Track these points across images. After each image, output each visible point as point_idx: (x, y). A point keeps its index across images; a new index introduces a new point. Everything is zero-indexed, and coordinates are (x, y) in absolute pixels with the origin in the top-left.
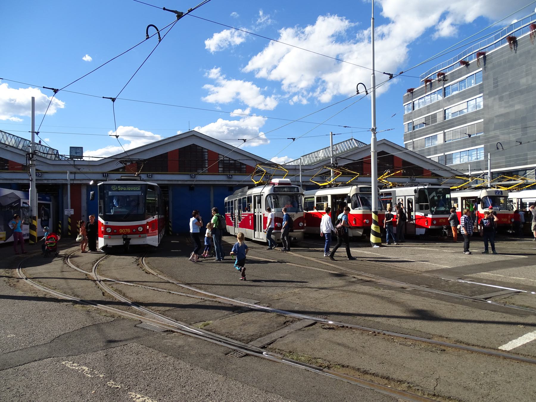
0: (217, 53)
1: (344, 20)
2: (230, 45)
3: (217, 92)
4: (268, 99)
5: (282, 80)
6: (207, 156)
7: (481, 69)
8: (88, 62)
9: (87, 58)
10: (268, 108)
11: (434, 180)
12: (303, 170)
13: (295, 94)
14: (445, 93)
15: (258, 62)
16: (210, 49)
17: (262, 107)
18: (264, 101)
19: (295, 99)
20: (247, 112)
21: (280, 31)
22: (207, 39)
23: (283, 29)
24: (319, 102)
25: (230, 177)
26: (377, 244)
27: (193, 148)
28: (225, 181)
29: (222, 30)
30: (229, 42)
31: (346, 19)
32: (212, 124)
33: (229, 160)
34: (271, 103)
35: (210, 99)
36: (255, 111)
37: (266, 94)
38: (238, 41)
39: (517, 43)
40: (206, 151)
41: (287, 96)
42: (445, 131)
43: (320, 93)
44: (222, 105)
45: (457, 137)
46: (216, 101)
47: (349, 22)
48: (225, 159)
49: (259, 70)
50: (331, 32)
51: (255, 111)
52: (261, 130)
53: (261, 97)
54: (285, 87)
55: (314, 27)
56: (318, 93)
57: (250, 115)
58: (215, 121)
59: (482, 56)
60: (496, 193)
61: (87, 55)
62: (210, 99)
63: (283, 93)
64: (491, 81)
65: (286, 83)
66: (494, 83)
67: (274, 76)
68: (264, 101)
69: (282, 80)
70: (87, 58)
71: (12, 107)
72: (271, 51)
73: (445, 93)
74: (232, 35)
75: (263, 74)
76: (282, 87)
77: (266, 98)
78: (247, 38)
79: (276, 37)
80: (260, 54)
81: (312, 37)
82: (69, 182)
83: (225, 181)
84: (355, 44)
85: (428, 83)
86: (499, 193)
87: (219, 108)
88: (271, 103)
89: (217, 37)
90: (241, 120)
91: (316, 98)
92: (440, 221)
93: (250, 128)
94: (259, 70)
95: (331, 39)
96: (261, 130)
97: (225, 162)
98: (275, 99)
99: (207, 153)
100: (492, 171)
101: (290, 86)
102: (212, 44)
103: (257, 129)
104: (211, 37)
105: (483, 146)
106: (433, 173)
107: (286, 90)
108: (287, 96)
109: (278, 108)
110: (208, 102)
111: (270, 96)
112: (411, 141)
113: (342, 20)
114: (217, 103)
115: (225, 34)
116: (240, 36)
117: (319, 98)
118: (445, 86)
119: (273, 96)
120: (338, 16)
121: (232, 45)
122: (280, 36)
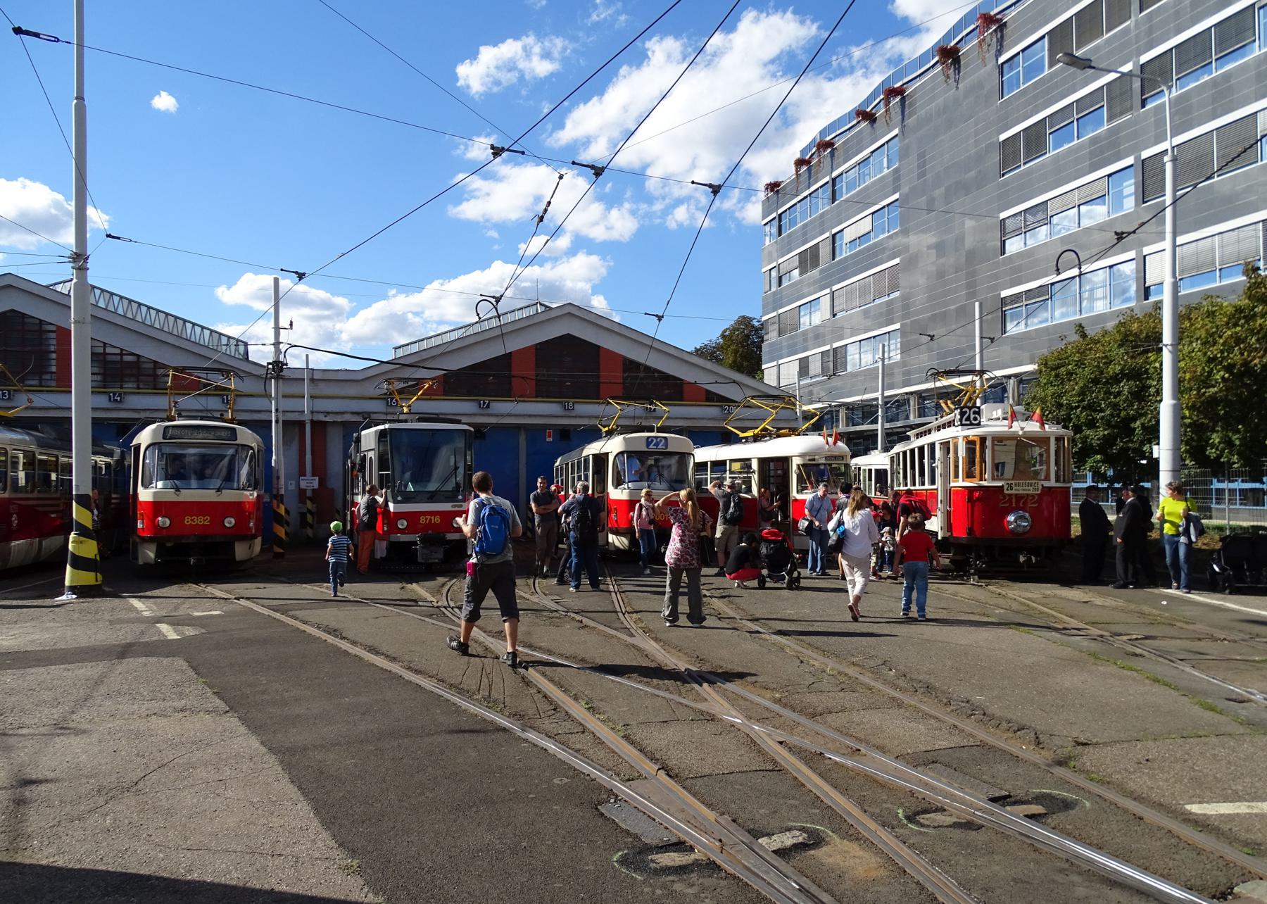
0: (488, 96)
1: (808, 22)
2: (522, 78)
3: (488, 194)
4: (614, 213)
5: (646, 166)
6: (54, 342)
7: (896, 131)
8: (164, 115)
9: (164, 102)
10: (615, 235)
11: (214, 403)
12: (312, 380)
13: (679, 202)
14: (834, 192)
15: (590, 122)
16: (468, 87)
17: (598, 233)
18: (605, 217)
19: (681, 214)
20: (563, 242)
21: (648, 44)
22: (462, 61)
23: (655, 39)
24: (739, 223)
25: (117, 399)
26: (73, 589)
27: (568, 341)
28: (475, 415)
29: (503, 41)
30: (520, 71)
31: (813, 21)
32: (478, 272)
33: (121, 354)
34: (622, 224)
35: (470, 210)
36: (582, 244)
37: (611, 201)
38: (542, 68)
39: (959, 62)
40: (53, 328)
41: (658, 207)
42: (834, 288)
43: (739, 201)
44: (501, 227)
45: (854, 304)
46: (483, 216)
47: (819, 28)
48: (108, 350)
49: (587, 142)
50: (772, 50)
51: (582, 244)
52: (596, 290)
53: (597, 209)
54: (651, 185)
55: (731, 36)
56: (735, 201)
57: (572, 252)
58: (485, 266)
59: (898, 99)
60: (648, 444)
61: (163, 94)
62: (470, 210)
63: (650, 200)
64: (913, 160)
65: (655, 172)
66: (919, 167)
67: (626, 158)
68: (605, 217)
69: (646, 166)
70: (164, 102)
71: (26, 223)
72: (627, 91)
73: (834, 192)
74: (527, 51)
75: (596, 152)
76: (647, 184)
77: (609, 209)
78: (565, 60)
79: (641, 59)
80: (595, 99)
81: (726, 62)
82: (307, 417)
83: (475, 415)
84: (830, 79)
85: (804, 168)
86: (657, 444)
87: (493, 234)
88: (622, 224)
89: (488, 55)
90: (548, 266)
91: (730, 214)
92: (423, 520)
93: (569, 284)
94: (587, 142)
95: (772, 68)
96: (596, 290)
97: (109, 358)
98: (633, 213)
99: (54, 335)
100: (887, 393)
101: (666, 179)
102: (475, 74)
103: (585, 287)
104: (473, 55)
105: (897, 326)
106: (708, 392)
107: (657, 194)
108: (658, 207)
109: (640, 234)
110: (462, 216)
111: (620, 205)
112: (774, 314)
113: (802, 22)
114: (487, 221)
115: (510, 48)
116: (546, 55)
117: (737, 214)
118: (835, 174)
119: (627, 205)
120: (794, 12)
121: (527, 77)
122: (647, 57)
